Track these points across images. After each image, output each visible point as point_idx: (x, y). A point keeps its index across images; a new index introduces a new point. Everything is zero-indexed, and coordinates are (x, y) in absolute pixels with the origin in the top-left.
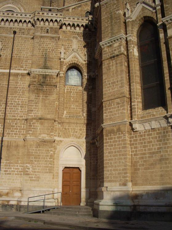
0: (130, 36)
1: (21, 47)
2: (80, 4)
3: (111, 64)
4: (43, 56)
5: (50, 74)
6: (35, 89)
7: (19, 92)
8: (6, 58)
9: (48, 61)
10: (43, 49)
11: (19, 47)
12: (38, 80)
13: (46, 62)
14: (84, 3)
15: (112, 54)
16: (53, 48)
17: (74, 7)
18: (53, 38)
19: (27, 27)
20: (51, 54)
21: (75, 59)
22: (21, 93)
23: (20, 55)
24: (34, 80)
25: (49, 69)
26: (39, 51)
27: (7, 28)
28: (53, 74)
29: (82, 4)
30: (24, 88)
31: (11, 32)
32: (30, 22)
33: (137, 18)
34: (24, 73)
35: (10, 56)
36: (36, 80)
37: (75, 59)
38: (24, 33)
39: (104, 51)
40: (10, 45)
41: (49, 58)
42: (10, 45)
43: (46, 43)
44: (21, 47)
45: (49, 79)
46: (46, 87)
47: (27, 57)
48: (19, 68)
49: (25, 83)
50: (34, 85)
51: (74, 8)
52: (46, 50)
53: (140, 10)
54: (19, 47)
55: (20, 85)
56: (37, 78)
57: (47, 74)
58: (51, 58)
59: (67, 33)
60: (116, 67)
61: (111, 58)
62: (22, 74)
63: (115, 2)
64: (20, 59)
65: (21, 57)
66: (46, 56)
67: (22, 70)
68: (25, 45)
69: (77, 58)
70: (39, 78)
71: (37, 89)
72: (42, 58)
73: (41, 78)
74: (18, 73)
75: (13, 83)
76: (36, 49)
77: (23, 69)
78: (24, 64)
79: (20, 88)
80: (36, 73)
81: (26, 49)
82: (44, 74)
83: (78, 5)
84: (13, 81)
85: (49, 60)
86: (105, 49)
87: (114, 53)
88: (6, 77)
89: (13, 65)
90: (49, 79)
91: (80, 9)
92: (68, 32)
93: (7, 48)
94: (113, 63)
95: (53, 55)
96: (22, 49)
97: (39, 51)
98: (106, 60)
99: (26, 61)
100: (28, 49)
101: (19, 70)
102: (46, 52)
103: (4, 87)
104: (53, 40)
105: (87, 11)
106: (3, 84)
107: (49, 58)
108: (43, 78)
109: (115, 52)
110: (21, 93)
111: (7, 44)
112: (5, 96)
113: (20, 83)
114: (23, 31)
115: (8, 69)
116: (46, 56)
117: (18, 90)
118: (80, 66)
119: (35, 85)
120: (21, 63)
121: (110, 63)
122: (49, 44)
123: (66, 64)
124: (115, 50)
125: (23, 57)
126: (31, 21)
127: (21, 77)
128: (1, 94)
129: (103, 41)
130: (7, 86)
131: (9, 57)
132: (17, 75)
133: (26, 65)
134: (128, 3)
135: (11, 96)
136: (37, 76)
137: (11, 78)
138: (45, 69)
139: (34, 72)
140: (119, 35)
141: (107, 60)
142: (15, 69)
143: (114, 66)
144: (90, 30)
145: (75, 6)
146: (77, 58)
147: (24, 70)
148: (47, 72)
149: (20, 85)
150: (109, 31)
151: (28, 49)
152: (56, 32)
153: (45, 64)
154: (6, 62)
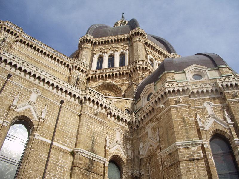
0: (207, 143)
1: (67, 119)
2: (121, 100)
3: (191, 166)
4: (91, 138)
5: (97, 160)
6: (80, 173)
7: (60, 172)
8: (49, 126)
9: (95, 146)
10: (91, 131)
11: (64, 119)
12: (84, 164)
13: (94, 146)
14: (125, 100)
15: (191, 156)
16: (100, 133)
17: (116, 100)
18: (101, 122)
19: (74, 102)
20: (98, 139)
21: (119, 152)
22: (61, 174)
23: (65, 128)
24: (80, 162)
25: (96, 154)
26: (87, 132)
27: (55, 94)
28: (100, 161)
29: (123, 100)
30: (66, 168)
31: (58, 100)
32: (79, 98)
33: (210, 129)
34: (67, 151)
35: (53, 125)
36: (82, 162)
37: (119, 152)
38: (70, 106)
39: (181, 152)
40: (56, 113)
41: (96, 142)
42: (55, 113)
43: (95, 126)
44: (67, 119)
45: (95, 166)
46: (93, 175)
47: (71, 133)
48: (62, 143)
49: (67, 163)
50: (80, 168)
51: (117, 101)
52: (94, 132)
53: (212, 123)
54: (64, 119)
55: (62, 163)
56: (84, 160)
57: (94, 159)
58: (98, 143)
59: (111, 123)
60: (198, 170)
61: (190, 160)
62: (65, 150)
63: (187, 110)
64: (64, 132)
65: (66, 131)
66: (93, 139)
67: (65, 146)
68: (70, 119)
69: (120, 151)
70: (86, 162)
71: (83, 174)
72: (90, 140)
73: (87, 162)
74: (60, 148)
75: (54, 158)
76: (85, 128)
77: (66, 145)
78: (68, 139)
79: (61, 166)
80: (83, 155)
81: (72, 124)
82: (91, 158)
83: (120, 100)
84: (54, 155)
85: (96, 145)
86: (182, 150)
87: (193, 156)
88: (46, 149)
89: (56, 137)
90: (95, 166)
91: (121, 103)
92: (112, 122)
93: (52, 115)
94: (193, 165)
95: (101, 140)
96: (67, 122)
97: (87, 132)
98: (185, 161)
99: (71, 138)
100: (74, 125)
101: (63, 145)
102: (94, 134)
103: (42, 159)
104: (101, 124)
105: (127, 108)
106: (41, 156)
107: (96, 142)
108: (90, 163)
109: (194, 155)
110: (61, 174)
111: (52, 110)
112: (42, 172)
113: (62, 161)
114: (70, 104)
115: (49, 139)
116: (93, 139)
117: (59, 169)
118: (122, 160)
119: (81, 168)
120: (65, 138)
121: (189, 165)
122: (97, 127)
123: (110, 154)
124: (194, 153)
125: (68, 132)
126: (81, 97)
127: (63, 154)
128: (38, 168)
129: (178, 141)
130: (46, 160)
131: (53, 126)
132: (59, 150)
133: (70, 142)
134: (198, 114)
135: (49, 173)
136: (84, 158)
137: (53, 151)
138: (92, 152)
139: (81, 152)
140: (195, 140)
141: (186, 162)
142: (58, 143)
143: (195, 169)
144: (131, 126)
145: (117, 100)
146: (120, 151)
147: (67, 146)
148: (95, 158)
149: (62, 163)
150: (184, 134)
151: (74, 125)
152: (104, 118)
153: (92, 148)
154: (48, 131)
